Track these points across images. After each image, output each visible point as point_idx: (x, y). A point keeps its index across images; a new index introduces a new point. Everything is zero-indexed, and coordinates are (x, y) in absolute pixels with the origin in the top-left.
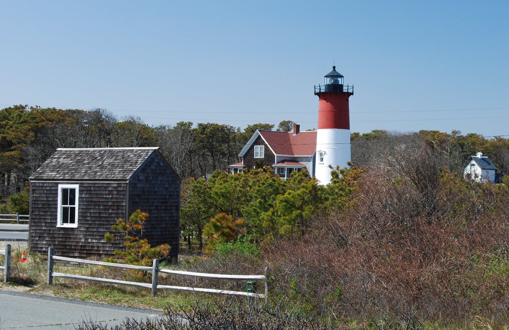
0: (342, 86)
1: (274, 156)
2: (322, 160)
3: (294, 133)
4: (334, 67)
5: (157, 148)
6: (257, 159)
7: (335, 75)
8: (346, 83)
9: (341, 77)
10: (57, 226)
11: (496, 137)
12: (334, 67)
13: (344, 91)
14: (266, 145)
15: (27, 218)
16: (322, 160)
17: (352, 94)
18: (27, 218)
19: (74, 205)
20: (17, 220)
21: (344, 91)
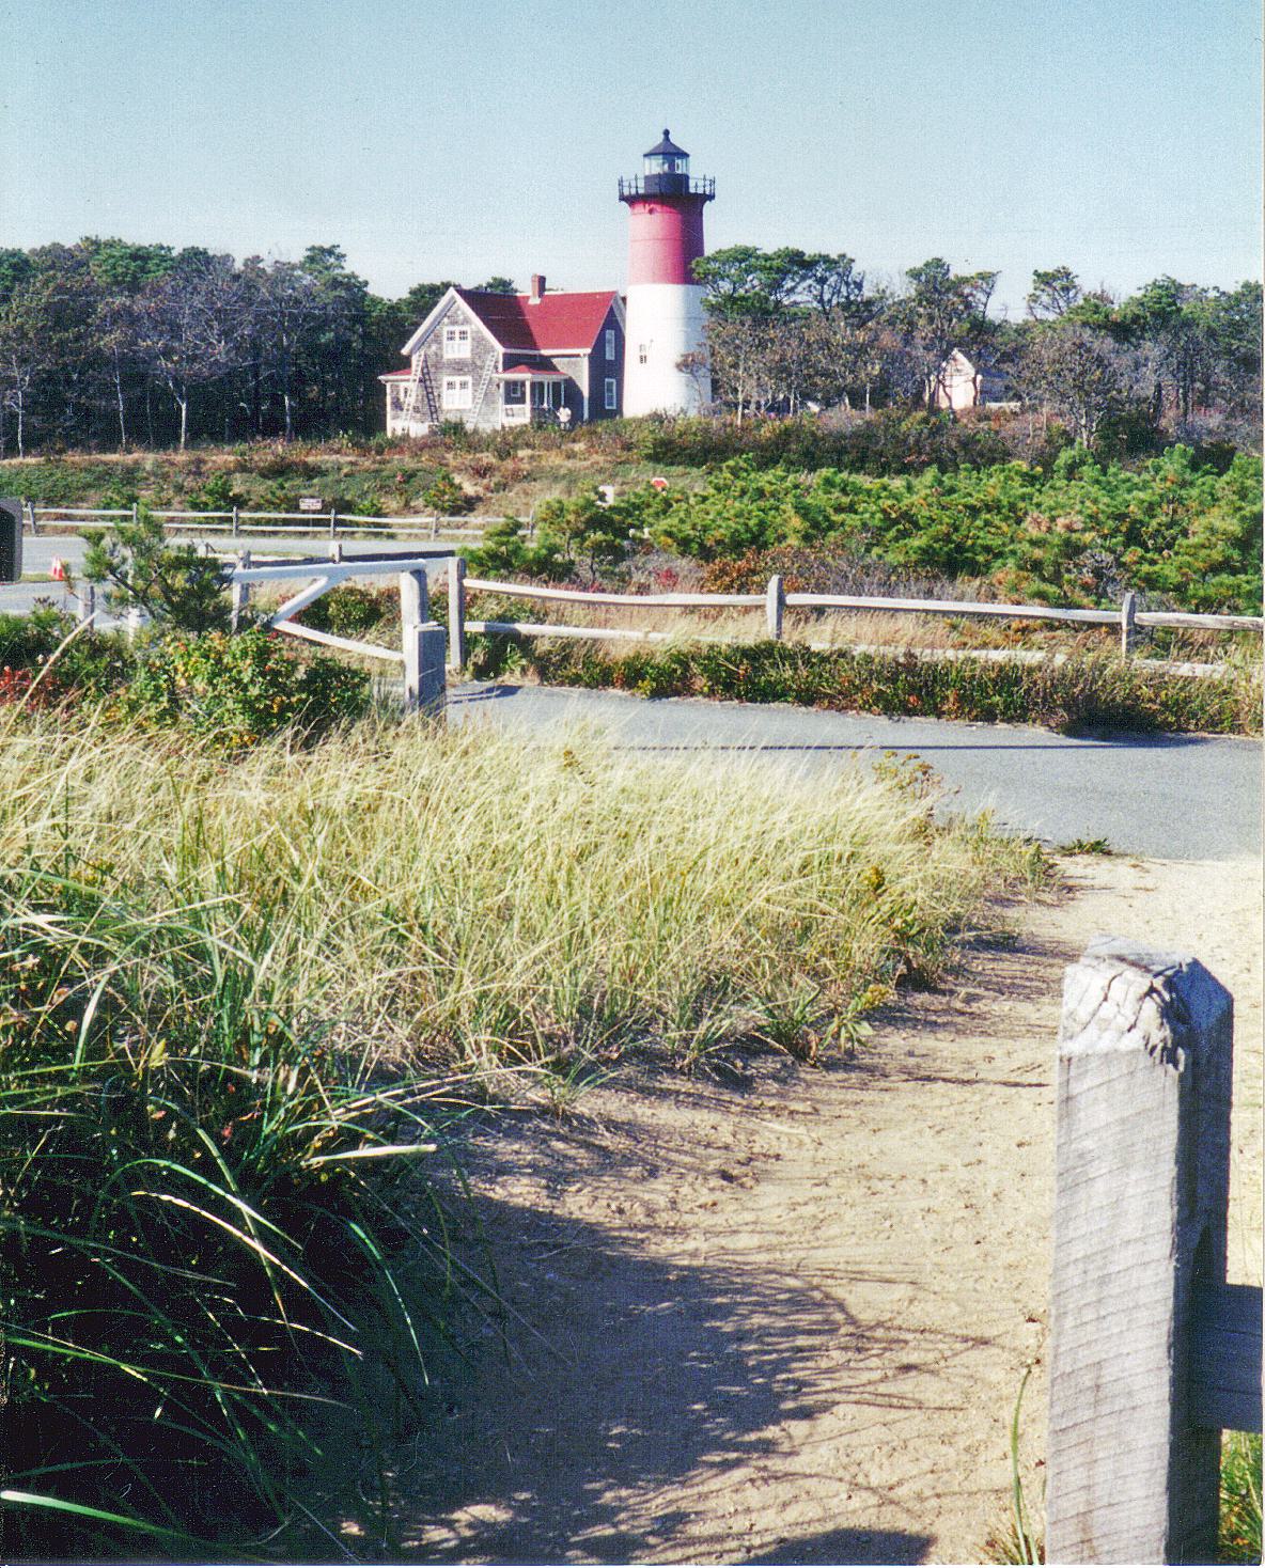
0: (686, 178)
2: (643, 359)
4: (666, 133)
7: (670, 152)
12: (666, 133)
13: (692, 190)
16: (643, 359)
17: (711, 197)
21: (692, 190)
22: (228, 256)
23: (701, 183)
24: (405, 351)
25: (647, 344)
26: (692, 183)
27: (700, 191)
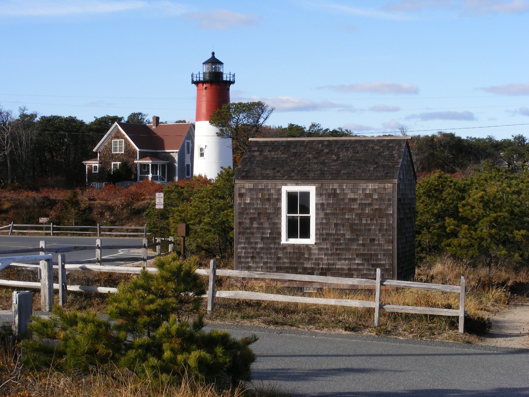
0: (222, 74)
1: (136, 151)
2: (202, 155)
3: (154, 125)
4: (213, 54)
5: (250, 139)
6: (116, 154)
7: (214, 61)
8: (226, 72)
9: (221, 63)
10: (282, 243)
11: (440, 133)
12: (213, 54)
13: (225, 79)
14: (126, 140)
15: (142, 231)
16: (202, 155)
17: (233, 82)
18: (142, 231)
19: (309, 213)
20: (51, 232)
21: (225, 79)
22: (260, 105)
23: (228, 76)
24: (94, 150)
25: (204, 148)
26: (224, 76)
27: (228, 79)
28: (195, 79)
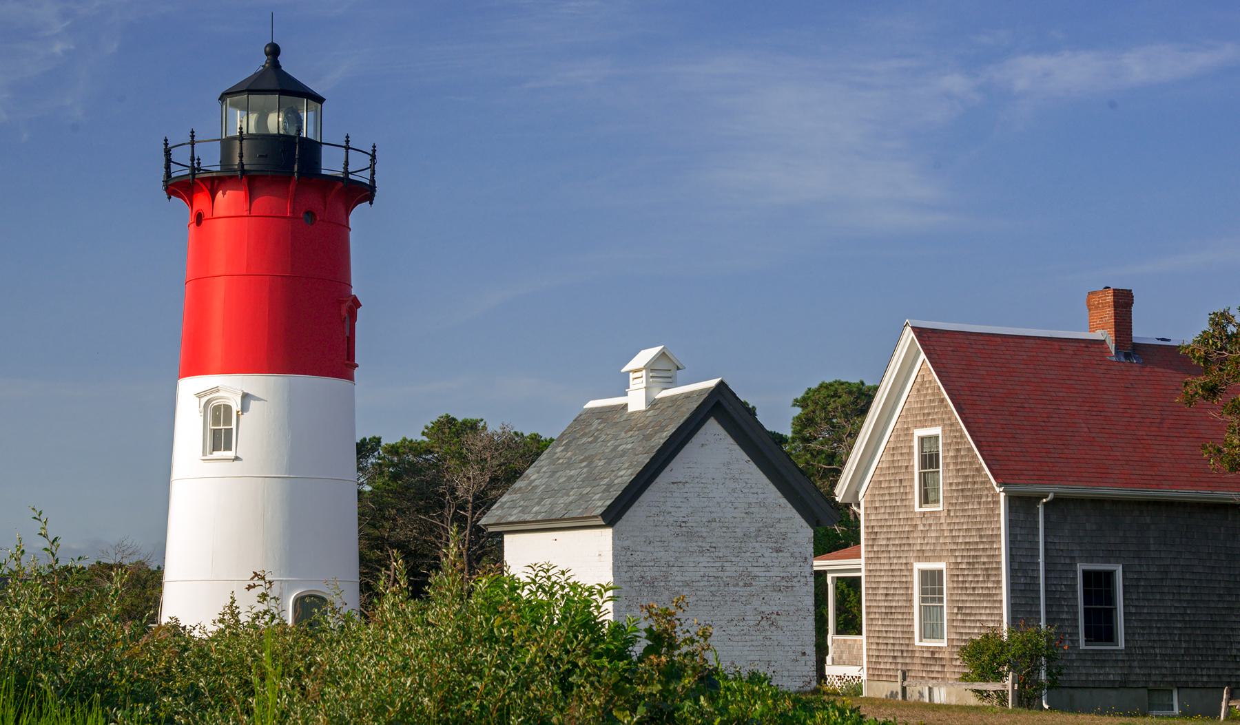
0: (311, 149)
4: (274, 51)
8: (340, 135)
12: (274, 51)
17: (366, 192)
28: (177, 172)
